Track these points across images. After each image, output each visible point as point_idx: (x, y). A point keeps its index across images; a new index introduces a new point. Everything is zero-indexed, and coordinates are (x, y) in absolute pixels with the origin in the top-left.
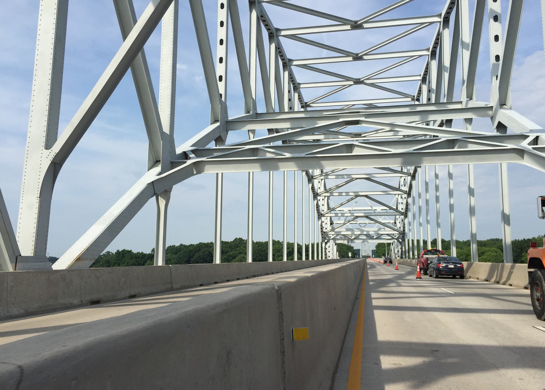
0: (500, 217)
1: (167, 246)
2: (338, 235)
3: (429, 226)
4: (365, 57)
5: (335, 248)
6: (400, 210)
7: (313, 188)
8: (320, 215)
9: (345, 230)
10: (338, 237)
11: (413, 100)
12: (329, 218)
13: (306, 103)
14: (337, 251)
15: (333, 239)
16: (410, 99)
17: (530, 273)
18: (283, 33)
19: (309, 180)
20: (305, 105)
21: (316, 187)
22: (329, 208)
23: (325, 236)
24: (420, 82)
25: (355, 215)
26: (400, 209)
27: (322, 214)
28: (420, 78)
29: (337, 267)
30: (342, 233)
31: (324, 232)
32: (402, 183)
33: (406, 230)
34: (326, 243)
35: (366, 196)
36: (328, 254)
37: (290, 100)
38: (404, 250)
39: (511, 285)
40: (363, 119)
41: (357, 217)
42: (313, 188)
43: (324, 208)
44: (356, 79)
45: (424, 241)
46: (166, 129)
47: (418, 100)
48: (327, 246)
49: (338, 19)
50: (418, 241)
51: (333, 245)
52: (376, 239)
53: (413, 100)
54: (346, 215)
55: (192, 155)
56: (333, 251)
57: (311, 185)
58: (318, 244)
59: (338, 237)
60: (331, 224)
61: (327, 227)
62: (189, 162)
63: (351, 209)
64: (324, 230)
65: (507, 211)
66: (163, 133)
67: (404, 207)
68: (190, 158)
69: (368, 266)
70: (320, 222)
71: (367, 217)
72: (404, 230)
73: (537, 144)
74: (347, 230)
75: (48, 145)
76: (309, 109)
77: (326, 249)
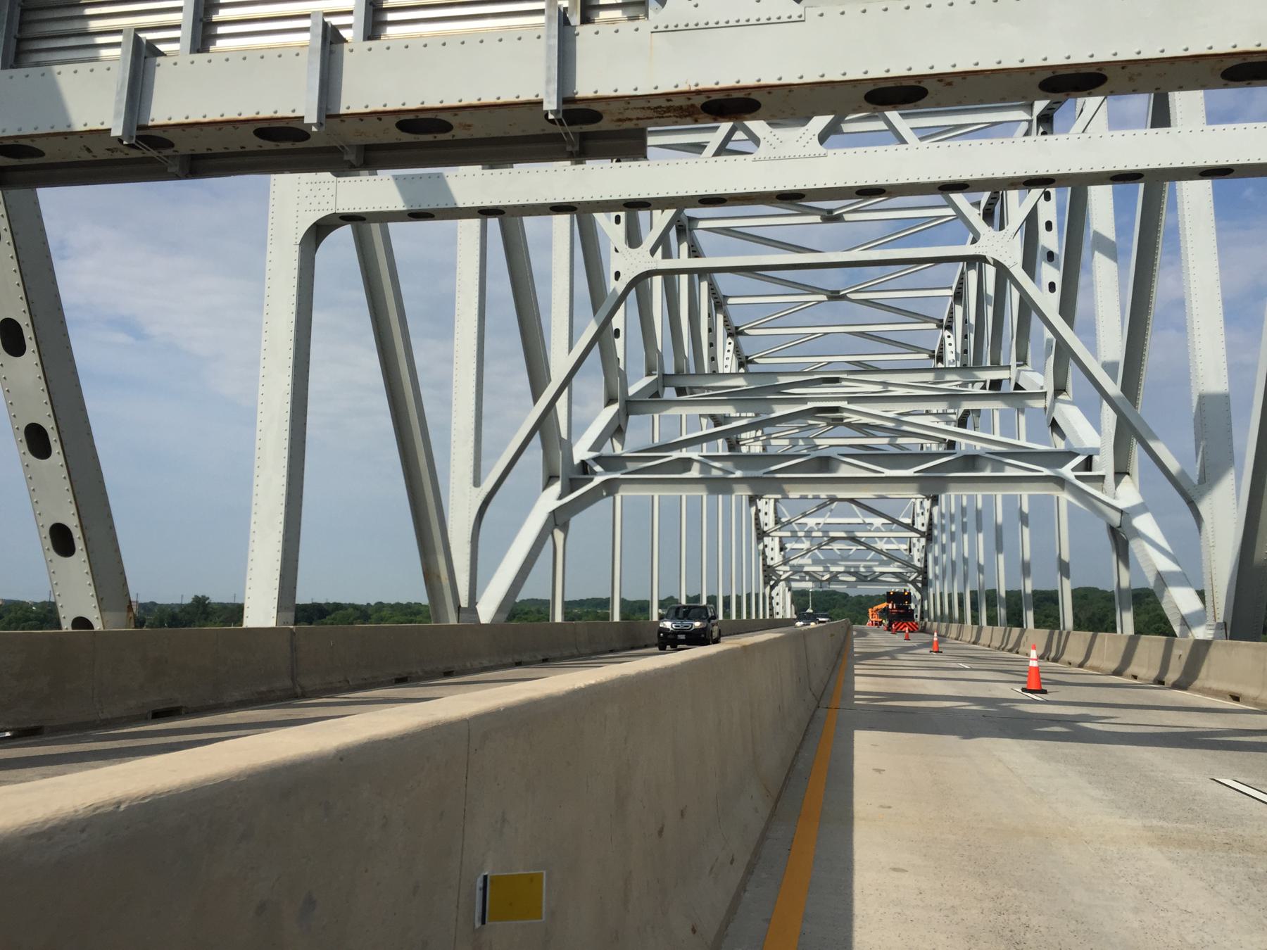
0: (1055, 565)
1: (523, 595)
4: (847, 217)
5: (788, 595)
8: (761, 534)
9: (810, 561)
11: (932, 357)
12: (777, 540)
13: (737, 328)
14: (792, 602)
15: (788, 580)
16: (925, 356)
17: (606, 603)
18: (702, 224)
20: (744, 362)
22: (777, 523)
23: (769, 573)
24: (951, 299)
25: (832, 534)
26: (918, 526)
28: (951, 293)
29: (778, 635)
30: (806, 569)
34: (772, 588)
35: (852, 501)
36: (777, 609)
37: (710, 330)
39: (1135, 677)
40: (844, 404)
41: (833, 539)
43: (768, 521)
44: (833, 292)
46: (564, 435)
47: (940, 359)
48: (774, 594)
53: (932, 357)
55: (598, 468)
56: (785, 603)
60: (782, 549)
61: (775, 557)
62: (598, 480)
64: (769, 562)
65: (1066, 557)
66: (561, 439)
67: (926, 521)
68: (595, 473)
70: (761, 547)
72: (926, 566)
73: (1090, 470)
74: (816, 562)
75: (477, 483)
76: (752, 368)
77: (771, 598)
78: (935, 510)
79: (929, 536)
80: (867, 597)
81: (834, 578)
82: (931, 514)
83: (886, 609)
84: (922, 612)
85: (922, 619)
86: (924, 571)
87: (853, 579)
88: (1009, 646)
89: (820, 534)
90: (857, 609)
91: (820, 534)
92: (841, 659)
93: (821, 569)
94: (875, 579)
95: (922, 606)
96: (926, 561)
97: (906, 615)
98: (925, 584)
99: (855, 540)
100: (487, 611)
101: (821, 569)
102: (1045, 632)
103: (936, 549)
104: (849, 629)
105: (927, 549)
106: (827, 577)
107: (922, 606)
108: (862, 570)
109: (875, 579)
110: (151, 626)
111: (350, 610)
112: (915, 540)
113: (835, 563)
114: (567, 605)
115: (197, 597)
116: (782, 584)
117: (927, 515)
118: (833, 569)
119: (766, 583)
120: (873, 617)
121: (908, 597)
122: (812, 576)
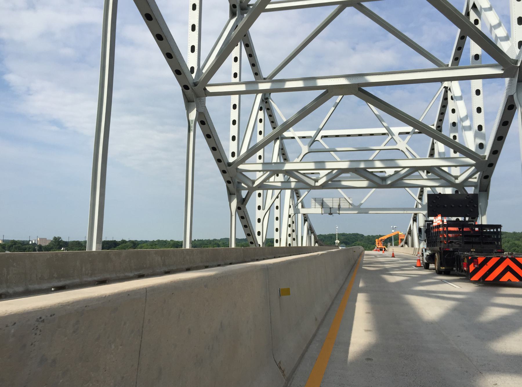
52: (392, 186)
80: (372, 236)
111: (128, 243)
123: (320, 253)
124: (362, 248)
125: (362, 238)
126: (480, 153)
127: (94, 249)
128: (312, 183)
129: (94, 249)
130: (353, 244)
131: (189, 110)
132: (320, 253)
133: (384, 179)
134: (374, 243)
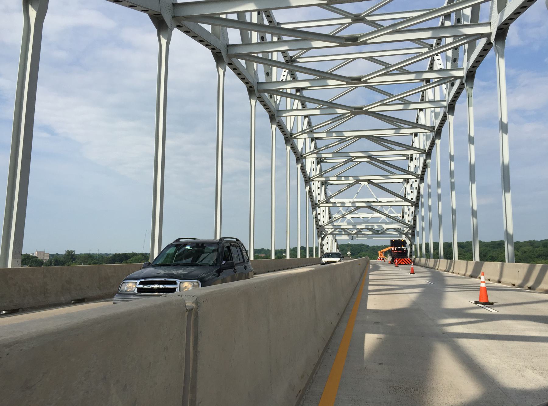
2: (336, 229)
3: (472, 147)
6: (407, 222)
7: (310, 191)
9: (346, 224)
10: (337, 232)
19: (313, 208)
21: (308, 170)
23: (321, 231)
25: (357, 204)
27: (316, 204)
30: (342, 227)
31: (320, 226)
32: (409, 191)
33: (418, 228)
34: (323, 239)
38: (414, 249)
41: (359, 207)
42: (303, 169)
43: (319, 196)
44: (355, 15)
45: (434, 243)
49: (342, 79)
50: (427, 245)
51: (332, 242)
52: (381, 234)
54: (346, 205)
57: (299, 166)
58: (317, 248)
59: (337, 232)
60: (330, 218)
61: (324, 219)
63: (351, 200)
64: (320, 223)
69: (371, 267)
71: (371, 207)
72: (415, 224)
77: (322, 245)
78: (422, 186)
79: (416, 204)
80: (377, 246)
81: (359, 232)
82: (419, 189)
83: (390, 251)
84: (411, 252)
85: (411, 256)
86: (413, 227)
87: (371, 233)
88: (530, 284)
89: (350, 205)
90: (373, 252)
91: (350, 205)
92: (358, 289)
93: (351, 227)
94: (383, 232)
95: (411, 249)
96: (415, 220)
97: (403, 254)
98: (413, 235)
99: (371, 207)
100: (156, 255)
101: (351, 227)
102: (464, 262)
103: (423, 211)
104: (368, 263)
105: (415, 214)
106: (355, 231)
107: (411, 249)
108: (376, 227)
109: (383, 232)
110: (46, 265)
111: (140, 256)
112: (406, 208)
113: (360, 224)
114: (256, 251)
115: (68, 251)
116: (330, 237)
117: (415, 192)
118: (358, 227)
119: (319, 236)
120: (381, 256)
121: (404, 243)
122: (346, 232)
123: (349, 261)
124: (250, 263)
125: (367, 249)
126: (409, 223)
127: (10, 266)
128: (351, 232)
129: (10, 266)
130: (359, 255)
131: (313, 211)
132: (349, 261)
133: (378, 231)
134: (377, 255)
